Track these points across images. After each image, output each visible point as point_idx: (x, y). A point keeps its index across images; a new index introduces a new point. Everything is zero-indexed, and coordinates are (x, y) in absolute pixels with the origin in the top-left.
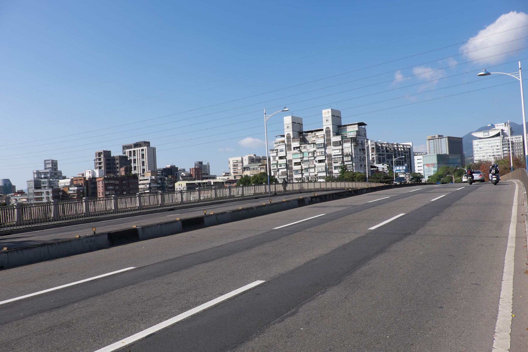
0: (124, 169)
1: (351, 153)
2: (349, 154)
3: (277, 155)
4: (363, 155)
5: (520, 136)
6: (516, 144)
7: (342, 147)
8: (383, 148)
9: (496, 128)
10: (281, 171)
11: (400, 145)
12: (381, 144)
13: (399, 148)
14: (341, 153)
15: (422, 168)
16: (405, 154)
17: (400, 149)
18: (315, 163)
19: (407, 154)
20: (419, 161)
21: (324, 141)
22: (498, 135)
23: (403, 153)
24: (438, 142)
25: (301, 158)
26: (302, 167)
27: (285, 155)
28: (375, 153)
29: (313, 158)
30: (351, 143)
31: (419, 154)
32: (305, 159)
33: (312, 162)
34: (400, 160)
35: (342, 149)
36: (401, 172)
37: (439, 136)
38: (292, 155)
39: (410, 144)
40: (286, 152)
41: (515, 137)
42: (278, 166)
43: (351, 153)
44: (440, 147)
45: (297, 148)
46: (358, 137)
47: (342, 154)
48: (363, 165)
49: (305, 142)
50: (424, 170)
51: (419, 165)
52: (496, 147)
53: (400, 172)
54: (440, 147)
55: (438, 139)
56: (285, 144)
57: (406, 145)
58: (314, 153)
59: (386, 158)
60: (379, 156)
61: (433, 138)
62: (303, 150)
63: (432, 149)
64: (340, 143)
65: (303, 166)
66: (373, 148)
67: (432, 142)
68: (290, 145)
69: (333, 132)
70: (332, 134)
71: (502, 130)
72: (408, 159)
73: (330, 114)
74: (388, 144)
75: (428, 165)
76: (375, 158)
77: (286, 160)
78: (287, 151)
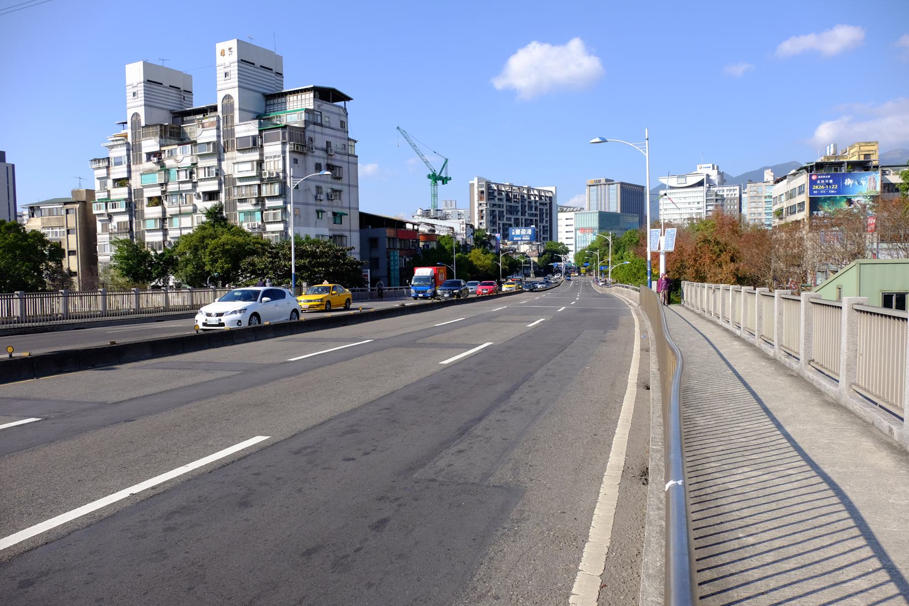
1: (281, 174)
2: (275, 175)
3: (108, 174)
4: (332, 183)
5: (735, 188)
7: (262, 155)
8: (502, 194)
10: (116, 219)
11: (533, 189)
12: (498, 185)
13: (532, 195)
14: (254, 174)
15: (572, 235)
16: (541, 207)
17: (532, 198)
18: (195, 201)
19: (545, 208)
20: (569, 222)
21: (218, 136)
22: (700, 184)
23: (538, 204)
24: (605, 191)
25: (161, 185)
26: (164, 212)
27: (125, 175)
28: (484, 202)
29: (189, 186)
30: (284, 144)
31: (569, 209)
32: (172, 187)
33: (188, 197)
34: (531, 218)
35: (260, 163)
36: (523, 239)
37: (607, 180)
38: (141, 174)
39: (553, 189)
40: (129, 166)
41: (728, 188)
42: (108, 204)
43: (281, 174)
44: (607, 199)
45: (155, 154)
46: (311, 127)
47: (259, 176)
48: (330, 215)
49: (182, 140)
50: (576, 239)
51: (569, 229)
52: (696, 205)
53: (522, 240)
54: (607, 199)
55: (605, 185)
56: (128, 144)
57: (544, 191)
58: (191, 173)
59: (505, 213)
60: (493, 209)
61: (597, 184)
62: (169, 163)
63: (594, 202)
64: (255, 144)
65: (168, 210)
66: (482, 192)
67: (594, 191)
68: (140, 148)
69: (240, 109)
70: (237, 113)
71: (708, 176)
72: (546, 217)
73: (234, 57)
74: (511, 186)
75: (583, 230)
76: (484, 212)
77: (130, 189)
78: (132, 163)
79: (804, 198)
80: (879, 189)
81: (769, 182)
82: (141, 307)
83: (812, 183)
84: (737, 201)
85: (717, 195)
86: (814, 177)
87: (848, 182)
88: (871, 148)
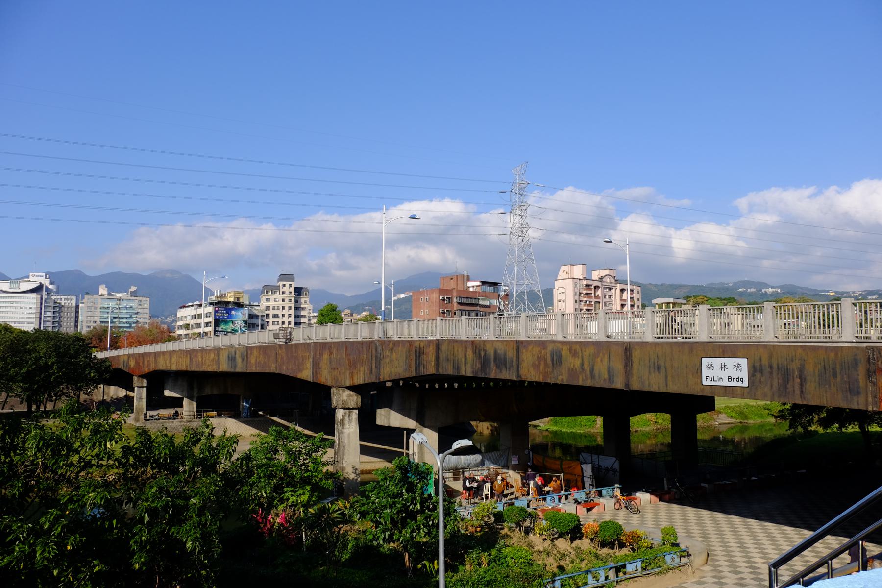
0: (538, 478)
5: (72, 298)
6: (66, 309)
9: (31, 278)
41: (66, 297)
79: (210, 319)
80: (247, 317)
81: (103, 295)
82: (597, 322)
83: (216, 312)
84: (74, 310)
85: (55, 303)
86: (217, 309)
87: (233, 312)
88: (240, 295)
